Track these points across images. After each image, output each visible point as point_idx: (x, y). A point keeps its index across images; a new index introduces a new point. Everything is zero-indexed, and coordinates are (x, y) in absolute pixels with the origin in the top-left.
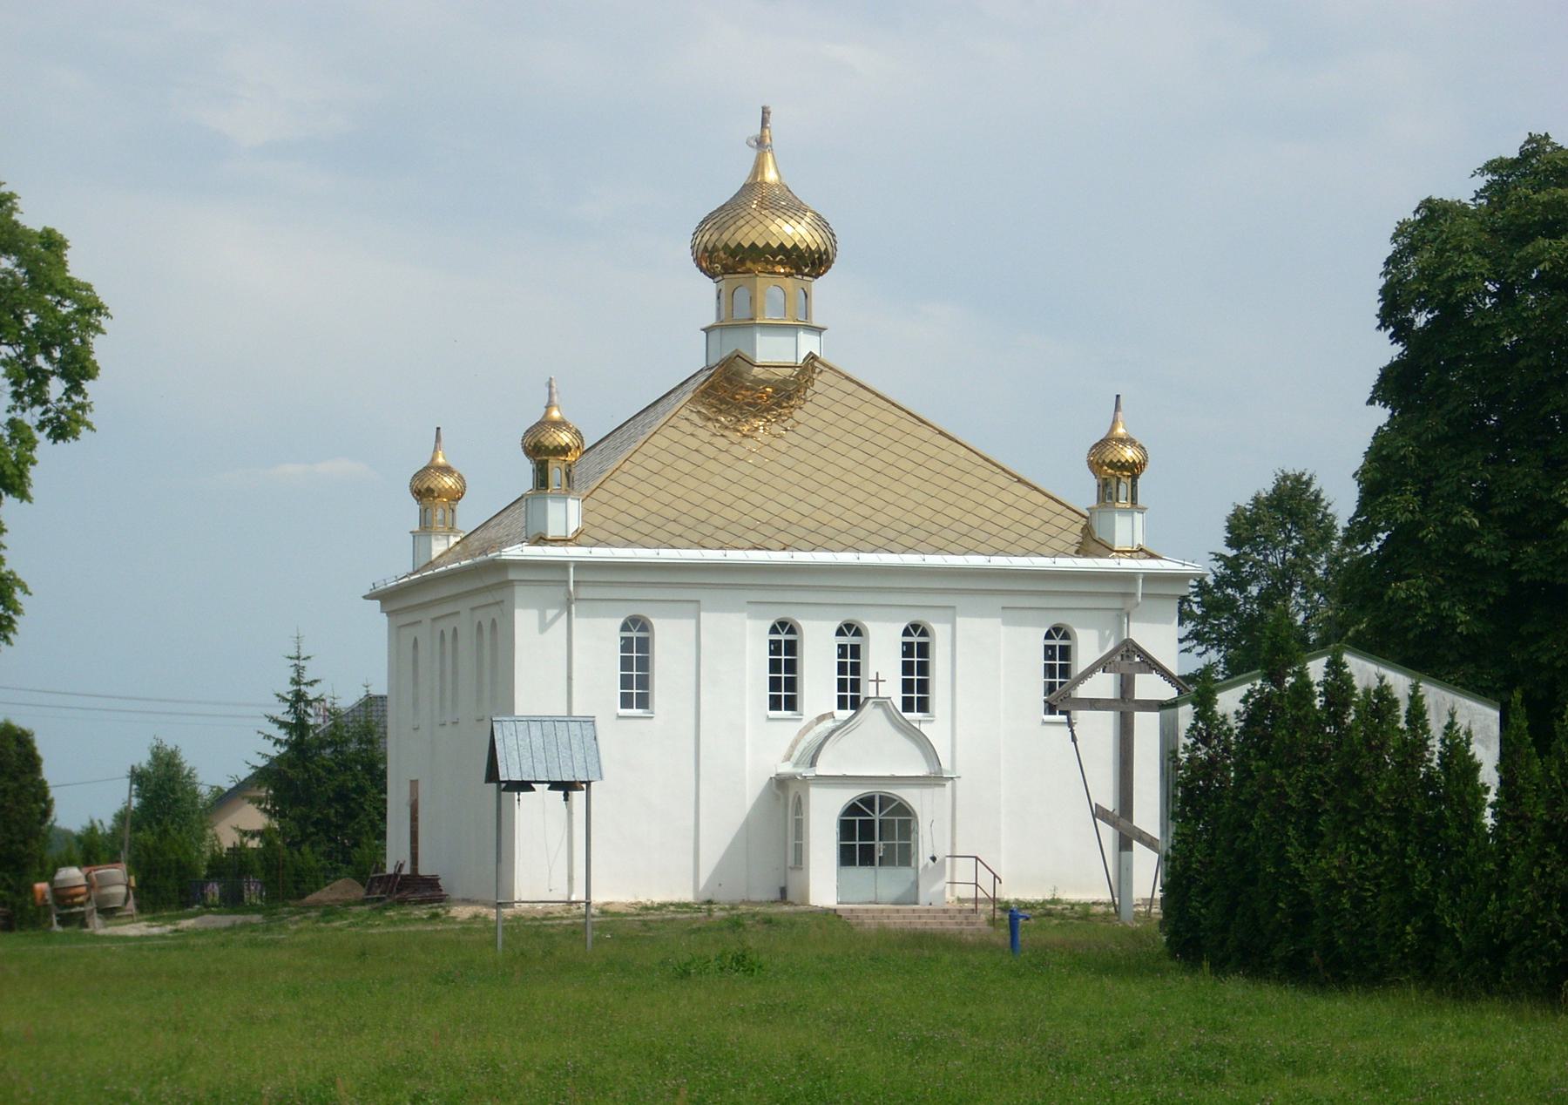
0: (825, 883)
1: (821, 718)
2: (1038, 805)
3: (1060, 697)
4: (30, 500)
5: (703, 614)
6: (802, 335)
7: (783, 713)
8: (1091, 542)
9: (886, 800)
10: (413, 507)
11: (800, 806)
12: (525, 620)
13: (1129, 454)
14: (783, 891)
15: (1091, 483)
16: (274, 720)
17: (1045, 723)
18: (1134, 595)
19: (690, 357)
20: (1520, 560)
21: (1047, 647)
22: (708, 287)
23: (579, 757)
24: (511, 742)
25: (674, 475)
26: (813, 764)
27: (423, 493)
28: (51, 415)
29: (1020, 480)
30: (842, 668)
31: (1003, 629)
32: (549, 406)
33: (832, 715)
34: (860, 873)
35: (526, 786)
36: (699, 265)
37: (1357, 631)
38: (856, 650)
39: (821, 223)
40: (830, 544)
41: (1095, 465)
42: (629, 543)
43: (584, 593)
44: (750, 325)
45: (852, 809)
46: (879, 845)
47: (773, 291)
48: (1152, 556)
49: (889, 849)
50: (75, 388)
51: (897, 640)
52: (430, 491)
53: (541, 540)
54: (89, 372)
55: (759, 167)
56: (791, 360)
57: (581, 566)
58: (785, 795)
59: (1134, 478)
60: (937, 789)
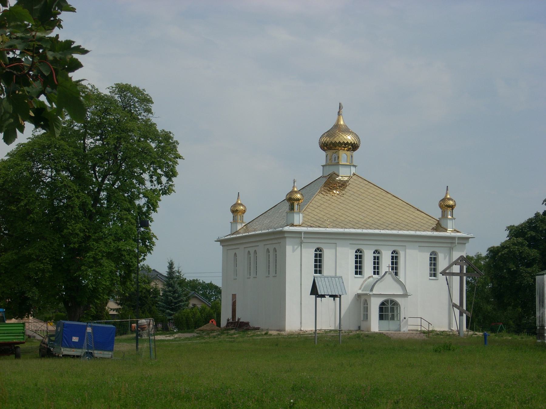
0: (375, 325)
1: (369, 277)
2: (432, 304)
3: (433, 273)
5: (337, 248)
6: (352, 167)
7: (358, 276)
8: (439, 227)
9: (392, 301)
10: (231, 215)
12: (289, 249)
13: (451, 203)
14: (359, 327)
15: (439, 211)
17: (430, 279)
18: (455, 243)
21: (430, 258)
22: (323, 153)
23: (339, 288)
24: (320, 283)
25: (324, 207)
26: (372, 290)
27: (234, 211)
28: (163, 187)
29: (418, 210)
30: (374, 263)
32: (294, 187)
33: (372, 276)
35: (323, 296)
36: (321, 148)
37: (502, 254)
38: (378, 258)
39: (356, 136)
40: (371, 227)
41: (441, 206)
44: (338, 164)
45: (383, 304)
47: (344, 155)
48: (458, 232)
50: (170, 179)
51: (372, 255)
52: (237, 210)
53: (292, 225)
54: (174, 174)
55: (338, 120)
57: (306, 233)
58: (362, 301)
59: (452, 209)
60: (406, 298)
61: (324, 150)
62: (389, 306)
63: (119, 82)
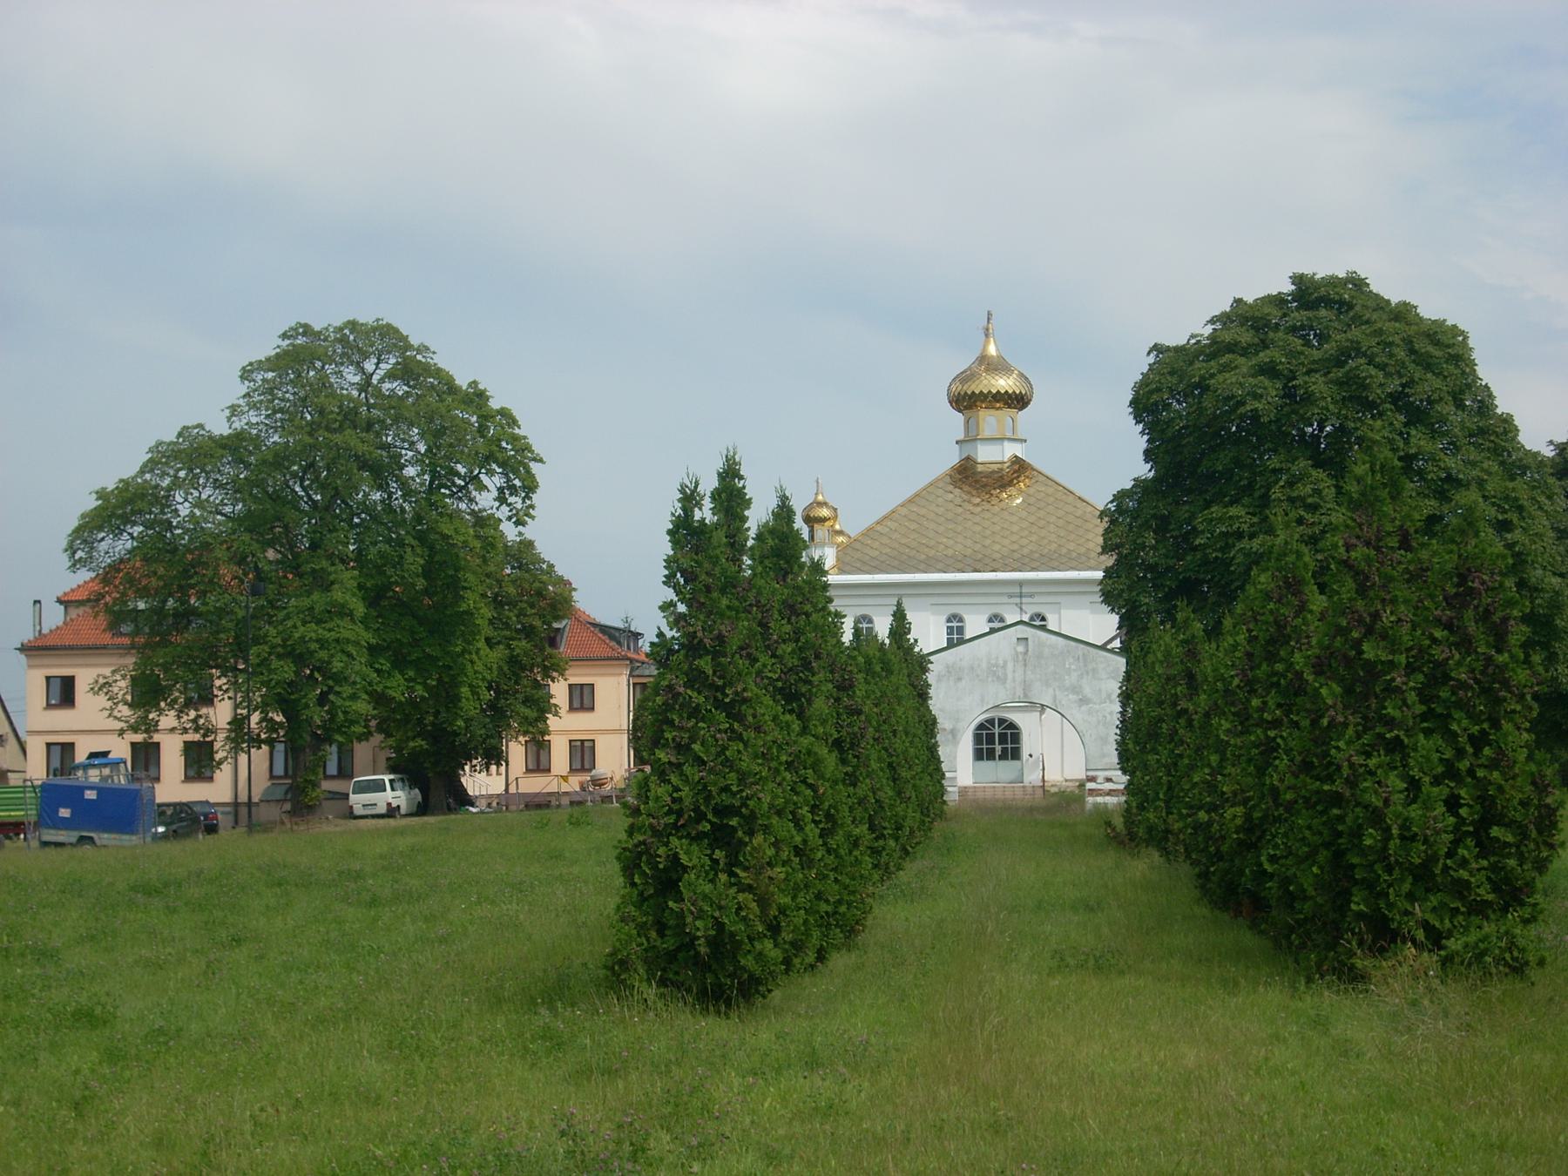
9: (1002, 721)
11: (340, 768)
19: (953, 458)
22: (959, 418)
31: (932, 618)
34: (986, 765)
46: (998, 748)
47: (990, 420)
49: (1004, 750)
55: (986, 343)
56: (999, 459)
61: (960, 411)
62: (997, 731)
63: (1307, 270)
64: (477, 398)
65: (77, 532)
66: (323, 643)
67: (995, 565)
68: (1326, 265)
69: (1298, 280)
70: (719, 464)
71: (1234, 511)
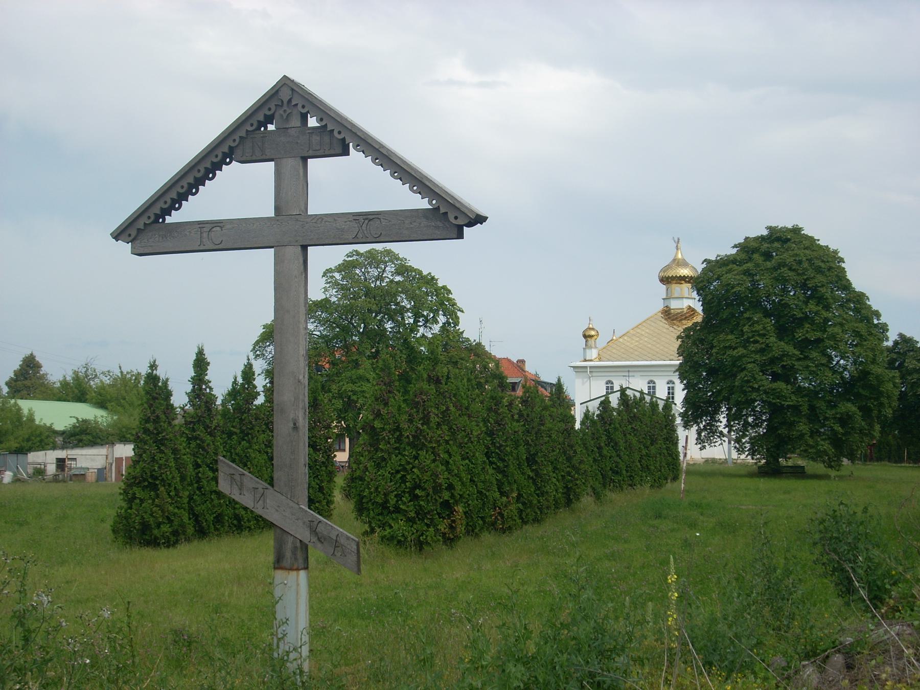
4: (118, 235)
16: (201, 364)
19: (660, 306)
20: (896, 368)
38: (673, 388)
42: (609, 360)
43: (594, 374)
53: (585, 360)
55: (677, 253)
57: (591, 367)
64: (430, 281)
65: (257, 343)
66: (355, 393)
67: (663, 357)
68: (785, 221)
69: (769, 228)
70: (196, 350)
71: (730, 337)
